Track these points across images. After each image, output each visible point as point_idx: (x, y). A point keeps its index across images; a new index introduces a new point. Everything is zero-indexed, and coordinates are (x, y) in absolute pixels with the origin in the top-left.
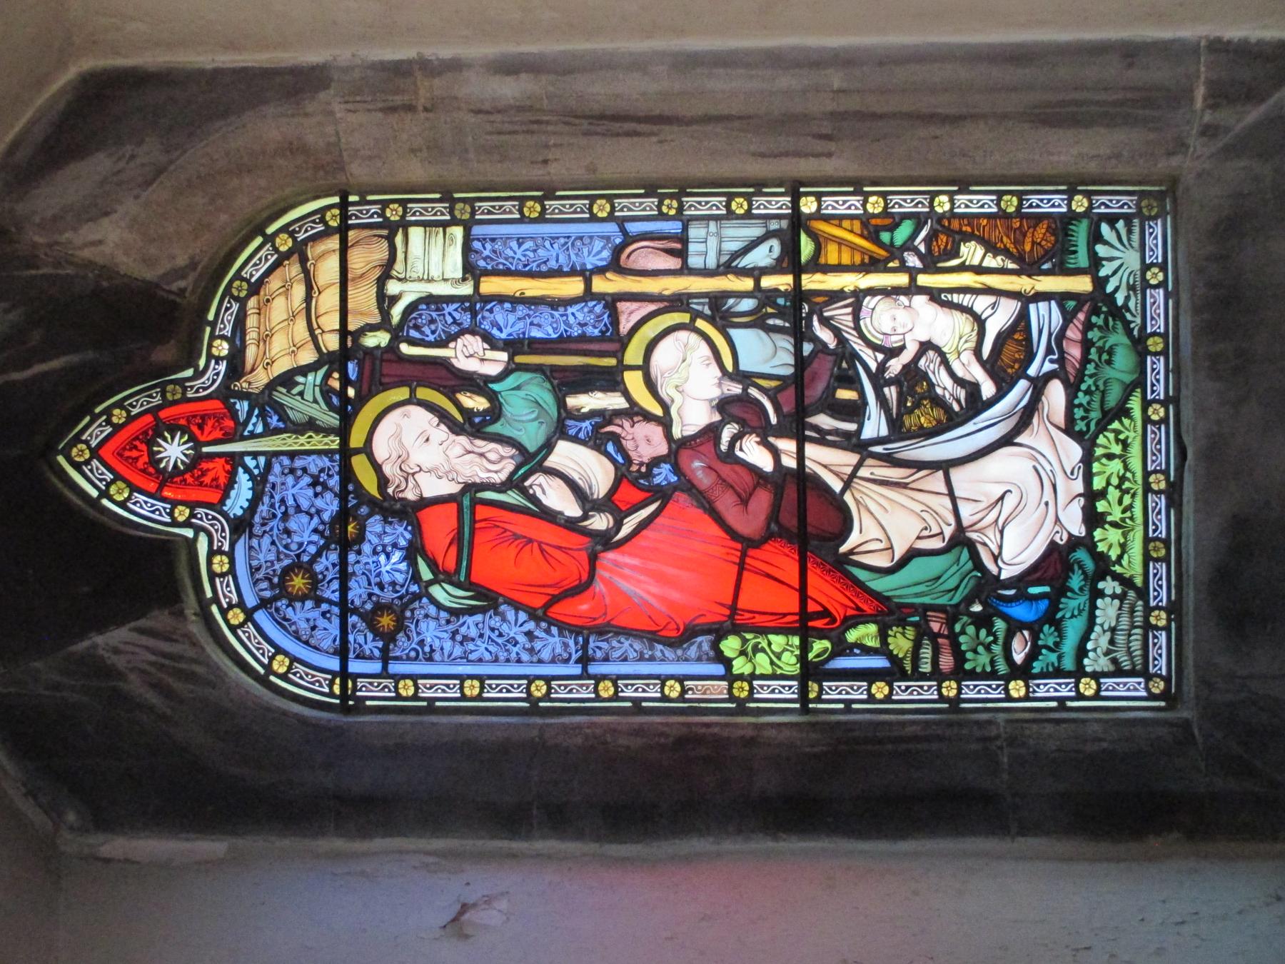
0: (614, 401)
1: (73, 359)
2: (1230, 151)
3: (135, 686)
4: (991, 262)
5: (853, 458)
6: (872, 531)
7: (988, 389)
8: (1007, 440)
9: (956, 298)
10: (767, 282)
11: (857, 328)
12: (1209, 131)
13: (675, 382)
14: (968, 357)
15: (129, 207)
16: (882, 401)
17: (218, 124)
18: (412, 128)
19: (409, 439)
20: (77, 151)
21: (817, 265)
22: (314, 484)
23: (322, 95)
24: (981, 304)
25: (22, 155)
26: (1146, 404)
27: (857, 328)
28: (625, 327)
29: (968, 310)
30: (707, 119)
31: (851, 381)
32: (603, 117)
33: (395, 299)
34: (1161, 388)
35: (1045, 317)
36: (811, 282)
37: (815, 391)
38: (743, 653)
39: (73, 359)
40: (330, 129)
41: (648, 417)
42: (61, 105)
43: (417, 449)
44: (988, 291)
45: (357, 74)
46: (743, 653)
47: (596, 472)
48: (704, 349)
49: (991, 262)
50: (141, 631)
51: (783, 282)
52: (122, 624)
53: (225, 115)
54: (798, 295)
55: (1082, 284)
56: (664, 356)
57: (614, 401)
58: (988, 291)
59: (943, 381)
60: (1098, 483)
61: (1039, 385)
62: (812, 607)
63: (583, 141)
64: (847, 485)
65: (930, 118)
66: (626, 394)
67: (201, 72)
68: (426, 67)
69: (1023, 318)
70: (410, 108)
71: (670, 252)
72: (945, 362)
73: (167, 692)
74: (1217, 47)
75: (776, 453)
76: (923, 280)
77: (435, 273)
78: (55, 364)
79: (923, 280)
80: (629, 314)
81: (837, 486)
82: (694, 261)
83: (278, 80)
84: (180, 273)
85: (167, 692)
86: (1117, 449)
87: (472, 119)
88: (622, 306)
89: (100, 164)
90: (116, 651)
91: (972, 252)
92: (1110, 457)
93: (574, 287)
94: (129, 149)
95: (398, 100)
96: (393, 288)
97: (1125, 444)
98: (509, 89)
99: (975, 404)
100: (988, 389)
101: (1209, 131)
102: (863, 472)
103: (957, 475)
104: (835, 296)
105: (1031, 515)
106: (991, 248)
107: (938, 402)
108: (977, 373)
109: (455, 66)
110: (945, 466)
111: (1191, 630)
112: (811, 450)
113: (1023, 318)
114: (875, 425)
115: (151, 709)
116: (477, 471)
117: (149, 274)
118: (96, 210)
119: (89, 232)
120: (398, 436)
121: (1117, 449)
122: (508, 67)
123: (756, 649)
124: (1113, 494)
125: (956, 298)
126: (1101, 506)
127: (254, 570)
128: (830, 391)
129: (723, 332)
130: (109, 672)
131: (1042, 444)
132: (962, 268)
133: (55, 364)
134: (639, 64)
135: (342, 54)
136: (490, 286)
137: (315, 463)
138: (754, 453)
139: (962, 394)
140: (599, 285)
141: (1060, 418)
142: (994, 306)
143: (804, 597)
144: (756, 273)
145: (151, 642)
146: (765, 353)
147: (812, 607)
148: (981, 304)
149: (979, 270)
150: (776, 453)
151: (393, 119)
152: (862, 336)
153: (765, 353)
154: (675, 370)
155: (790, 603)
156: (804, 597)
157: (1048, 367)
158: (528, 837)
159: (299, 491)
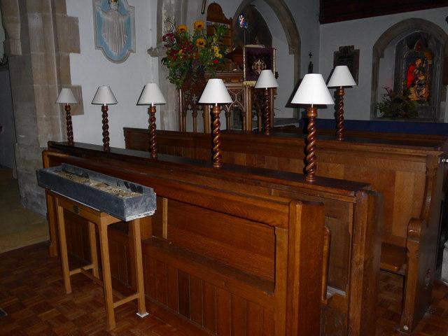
43: (419, 62)
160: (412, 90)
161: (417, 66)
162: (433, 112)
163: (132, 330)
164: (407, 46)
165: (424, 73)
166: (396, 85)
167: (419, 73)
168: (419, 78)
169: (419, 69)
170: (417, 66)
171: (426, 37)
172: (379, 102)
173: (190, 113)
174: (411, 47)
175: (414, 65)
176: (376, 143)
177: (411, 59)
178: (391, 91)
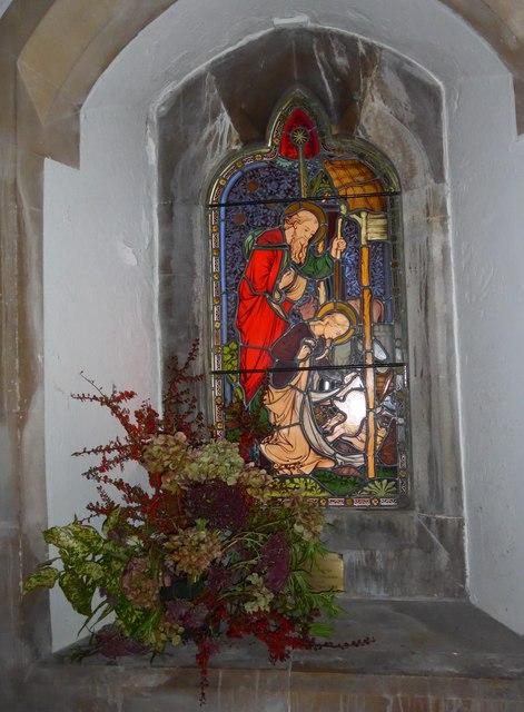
0: (322, 300)
1: (330, 95)
2: (420, 528)
3: (209, 129)
4: (379, 439)
5: (303, 389)
6: (277, 396)
7: (330, 439)
8: (311, 446)
9: (364, 427)
10: (369, 356)
11: (352, 390)
12: (428, 521)
13: (331, 321)
14: (342, 431)
15: (387, 110)
16: (326, 399)
17: (420, 141)
18: (421, 217)
19: (306, 224)
20: (408, 88)
21: (377, 374)
22: (289, 190)
23: (432, 181)
24: (363, 436)
25: (407, 67)
26: (326, 499)
27: (352, 390)
28: (352, 303)
29: (360, 431)
30: (427, 327)
31: (332, 386)
32: (427, 287)
33: (359, 215)
34: (333, 504)
35: (358, 460)
36: (370, 373)
37: (327, 373)
38: (231, 350)
39: (330, 95)
40: (420, 184)
41: (317, 312)
42: (427, 80)
43: (303, 228)
44: (368, 439)
45: (441, 193)
46: (231, 350)
47: (296, 295)
48: (343, 332)
49: (379, 439)
50: (230, 130)
51: (369, 362)
52: (233, 122)
53: (424, 143)
54: (364, 367)
55: (371, 474)
56: (340, 318)
57: (322, 300)
58: (368, 439)
59: (334, 422)
60: (296, 480)
61: (332, 458)
62: (248, 375)
63: (418, 281)
64: (292, 387)
65: (430, 413)
66: (325, 304)
67: (441, 133)
68: (444, 220)
69: (357, 451)
70: (428, 214)
71: (380, 318)
72: (340, 423)
73: (207, 142)
74: (461, 523)
75: (304, 360)
76: (371, 414)
77: (369, 230)
78: (328, 89)
79: (371, 414)
80: (355, 304)
81: (293, 383)
82: (376, 328)
83: (431, 115)
84: (364, 132)
85: (207, 142)
86: (309, 487)
87: (425, 238)
88: (358, 302)
89: (403, 97)
90: (222, 120)
91: (382, 433)
92: (306, 485)
93: (365, 282)
94: (410, 108)
95: (431, 209)
96: (363, 215)
97: (311, 490)
98: (436, 252)
99: (325, 434)
100: (330, 439)
101: (428, 521)
102: (298, 393)
103: (297, 428)
104: (364, 379)
105: (284, 455)
106: (384, 440)
107: (325, 420)
108: (336, 435)
109: (445, 231)
110: (301, 424)
111: (193, 72)
112: (306, 373)
113: (357, 451)
114: (316, 397)
115: (201, 136)
116: (296, 248)
117: (363, 121)
118: (386, 98)
119: (377, 97)
120: (308, 220)
121: (309, 487)
122: (445, 250)
123: (233, 355)
124: (292, 486)
125: (364, 427)
126: (288, 481)
127: (257, 169)
128: (328, 380)
129: (350, 339)
130: (214, 117)
131: (310, 459)
132: (376, 429)
133: (328, 89)
134: (447, 301)
135: (448, 187)
136: (365, 252)
137: (296, 189)
138: (304, 351)
139: (328, 429)
140: (366, 292)
141: (320, 466)
142: (362, 441)
143: (252, 371)
144: (372, 351)
145: (226, 133)
146: (342, 355)
147: (248, 375)
148: (363, 436)
149: (376, 435)
150: (304, 360)
151: (424, 207)
152: (349, 392)
153: (342, 355)
154: (335, 321)
155: (250, 366)
156: (252, 371)
157: (339, 461)
158: (160, 273)
159: (286, 184)
160: (279, 403)
161: (298, 254)
162: (443, 557)
163: (97, 599)
164: (225, 121)
165: (339, 292)
166: (177, 374)
167: (310, 294)
168: (317, 330)
169: (311, 267)
170: (298, 254)
171: (341, 61)
172: (59, 518)
173: (422, 707)
174: (252, 127)
175: (276, 247)
176: (44, 14)
177: (254, 204)
178: (147, 417)
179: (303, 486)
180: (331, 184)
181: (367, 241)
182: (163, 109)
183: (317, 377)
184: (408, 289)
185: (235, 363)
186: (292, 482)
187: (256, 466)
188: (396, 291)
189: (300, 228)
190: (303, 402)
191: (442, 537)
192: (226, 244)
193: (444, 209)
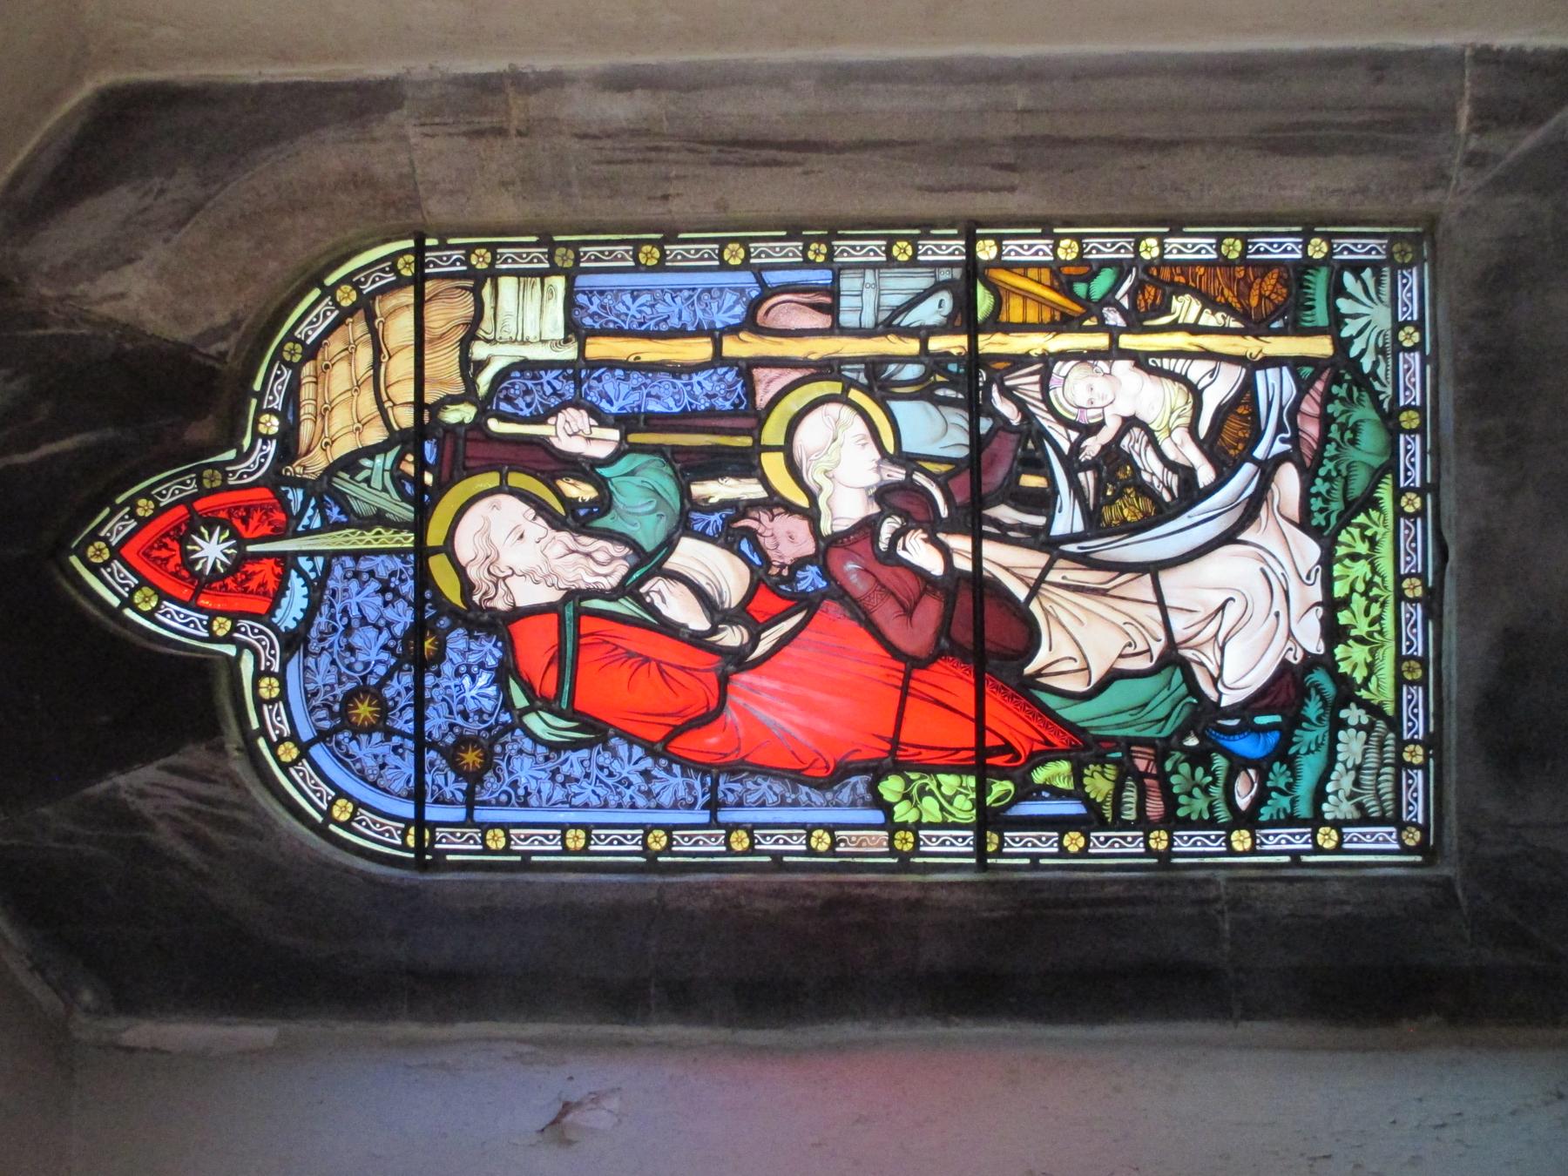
0: (749, 489)
1: (90, 437)
2: (1501, 185)
3: (165, 836)
4: (1209, 319)
5: (1041, 559)
6: (1065, 648)
7: (1205, 475)
8: (1229, 537)
9: (1166, 364)
10: (936, 344)
11: (1046, 400)
12: (1475, 160)
13: (823, 465)
14: (1181, 435)
15: (158, 252)
16: (1077, 489)
17: (266, 151)
18: (502, 156)
19: (499, 536)
20: (94, 185)
21: (996, 324)
22: (383, 591)
25: (27, 189)
26: (1398, 493)
27: (1046, 400)
29: (1181, 379)
30: (863, 145)
31: (1038, 465)
32: (735, 142)
33: (481, 365)
34: (1416, 473)
35: (1275, 387)
36: (990, 344)
37: (994, 478)
38: (906, 796)
39: (90, 437)
40: (402, 158)
41: (791, 508)
42: (75, 128)
43: (509, 547)
44: (1206, 355)
45: (435, 91)
46: (906, 796)
47: (727, 575)
48: (860, 426)
49: (1209, 319)
50: (172, 770)
51: (955, 344)
52: (149, 761)
53: (274, 140)
54: (974, 360)
55: (1321, 347)
56: (810, 435)
57: (749, 489)
58: (1206, 355)
59: (1150, 465)
60: (1340, 590)
61: (1267, 470)
62: (991, 740)
63: (712, 172)
64: (1034, 591)
65: (1135, 144)
66: (764, 481)
67: (246, 88)
68: (520, 82)
69: (1248, 388)
70: (501, 132)
71: (818, 307)
72: (1153, 442)
73: (204, 845)
74: (1486, 57)
75: (946, 553)
76: (1126, 341)
77: (531, 333)
78: (67, 444)
79: (1126, 341)
80: (768, 384)
81: (1021, 592)
82: (847, 319)
84: (219, 333)
85: (204, 845)
86: (1362, 548)
87: (576, 145)
88: (759, 373)
89: (122, 200)
90: (142, 794)
91: (1186, 308)
92: (1355, 557)
93: (700, 350)
95: (486, 121)
96: (479, 351)
97: (1373, 542)
98: (621, 109)
99: (1190, 493)
100: (1205, 475)
101: (1475, 160)
102: (1053, 576)
103: (1167, 579)
104: (1019, 361)
105: (1259, 628)
106: (1209, 302)
107: (1145, 490)
109: (555, 80)
110: (1153, 569)
112: (990, 549)
113: (1248, 388)
114: (1068, 519)
115: (185, 864)
116: (582, 575)
117: (182, 335)
118: (117, 256)
119: (108, 283)
120: (485, 532)
121: (1362, 548)
122: (620, 82)
123: (923, 792)
124: (1358, 602)
125: (1166, 364)
126: (1343, 617)
127: (309, 696)
128: (1013, 477)
129: (882, 405)
130: (133, 820)
131: (1271, 541)
132: (1174, 327)
133: (67, 444)
134: (780, 78)
136: (598, 348)
137: (384, 565)
138: (920, 553)
139: (1174, 480)
140: (731, 348)
141: (1293, 510)
142: (1213, 373)
143: (981, 728)
144: (923, 333)
145: (184, 783)
146: (933, 431)
147: (991, 740)
148: (1197, 371)
149: (1195, 329)
150: (946, 553)
152: (1051, 410)
153: (933, 431)
154: (823, 451)
155: (965, 735)
156: (981, 728)
157: (1279, 447)
158: (644, 1021)
179: (1362, 568)
180: (371, 452)
181: (566, 341)
182: (87, 997)
183: (1005, 513)
184: (729, 1031)
185: (949, 782)
186: (1345, 603)
187: (1263, 767)
188: (722, 454)
189: (514, 556)
190: (1087, 561)
191: (1527, 116)
192: (552, 806)
193: (487, 85)
